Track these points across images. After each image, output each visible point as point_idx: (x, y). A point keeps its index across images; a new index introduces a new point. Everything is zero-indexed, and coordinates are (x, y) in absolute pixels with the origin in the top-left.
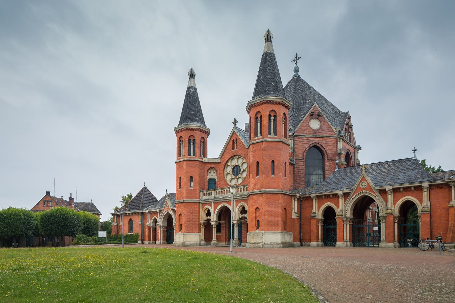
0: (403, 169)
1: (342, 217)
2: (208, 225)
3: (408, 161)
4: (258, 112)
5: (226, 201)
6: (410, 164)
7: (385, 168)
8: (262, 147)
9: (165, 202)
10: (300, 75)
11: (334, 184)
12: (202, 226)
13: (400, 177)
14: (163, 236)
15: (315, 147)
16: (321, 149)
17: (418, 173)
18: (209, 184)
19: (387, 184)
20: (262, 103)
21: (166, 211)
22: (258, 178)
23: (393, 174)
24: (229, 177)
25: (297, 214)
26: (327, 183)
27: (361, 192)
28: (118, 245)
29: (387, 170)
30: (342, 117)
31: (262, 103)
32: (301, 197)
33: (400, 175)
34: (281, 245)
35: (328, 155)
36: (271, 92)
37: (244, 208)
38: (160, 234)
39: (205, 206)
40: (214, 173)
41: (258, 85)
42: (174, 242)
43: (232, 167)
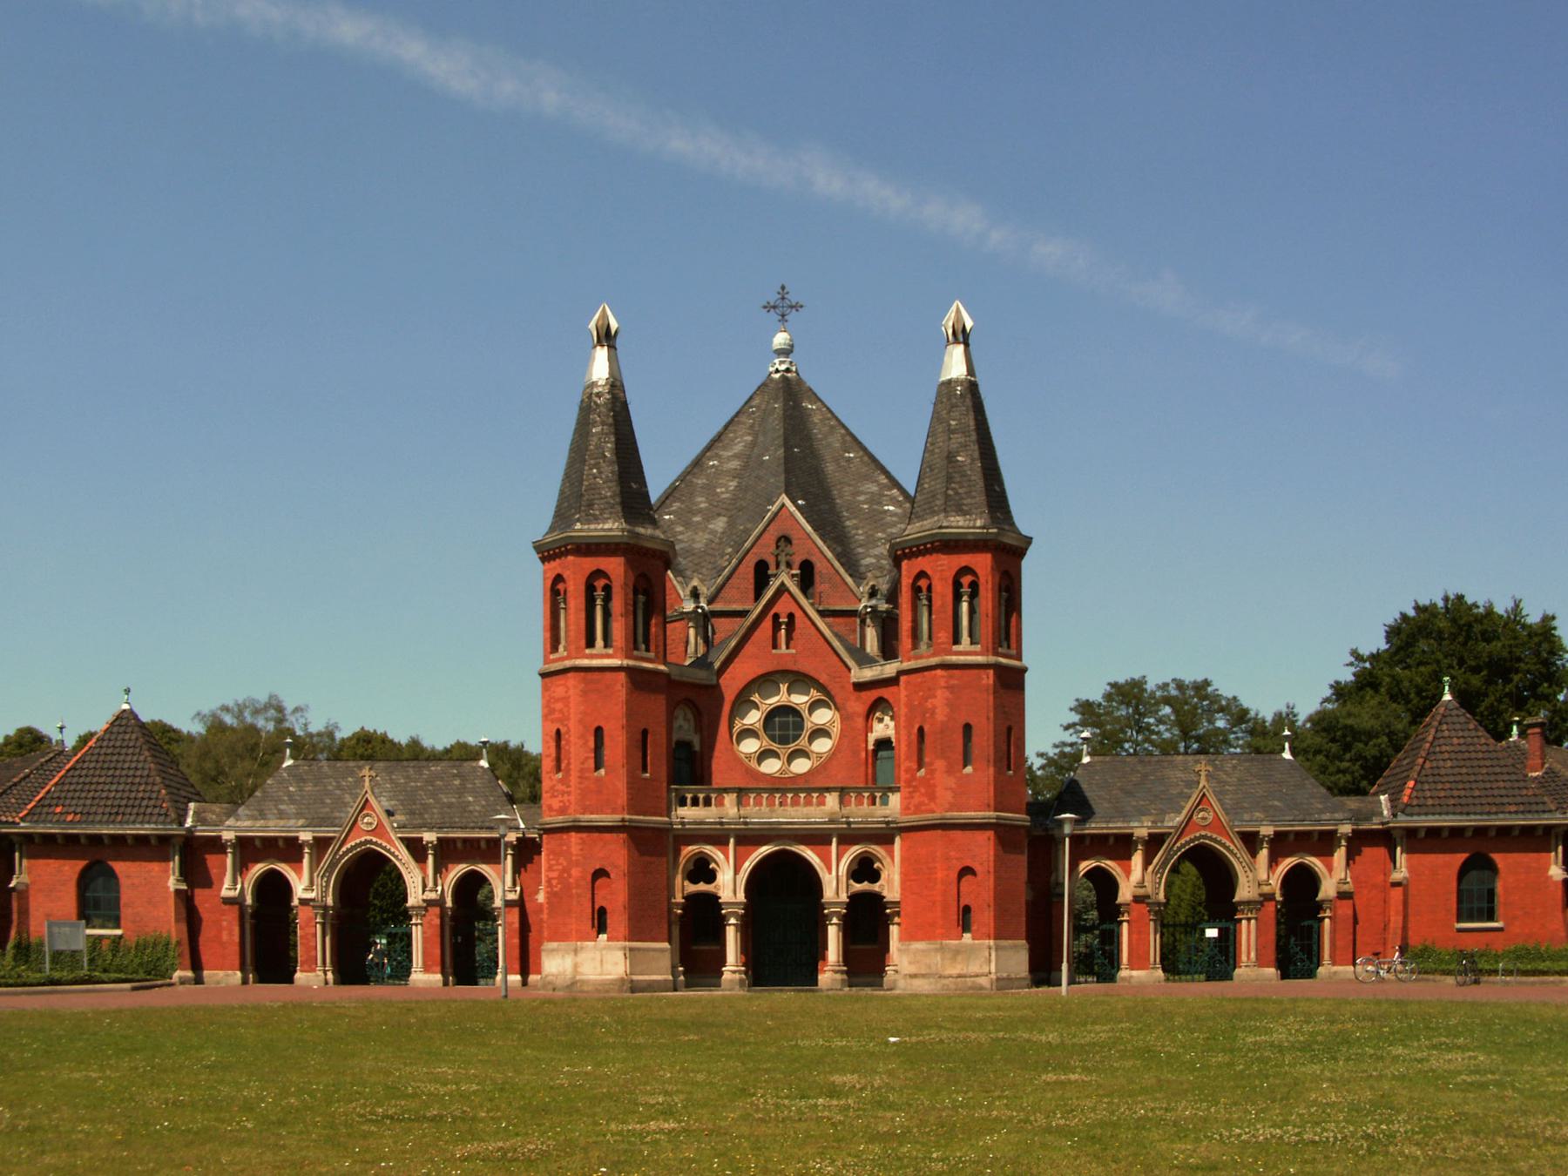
21: (358, 841)
28: (28, 993)
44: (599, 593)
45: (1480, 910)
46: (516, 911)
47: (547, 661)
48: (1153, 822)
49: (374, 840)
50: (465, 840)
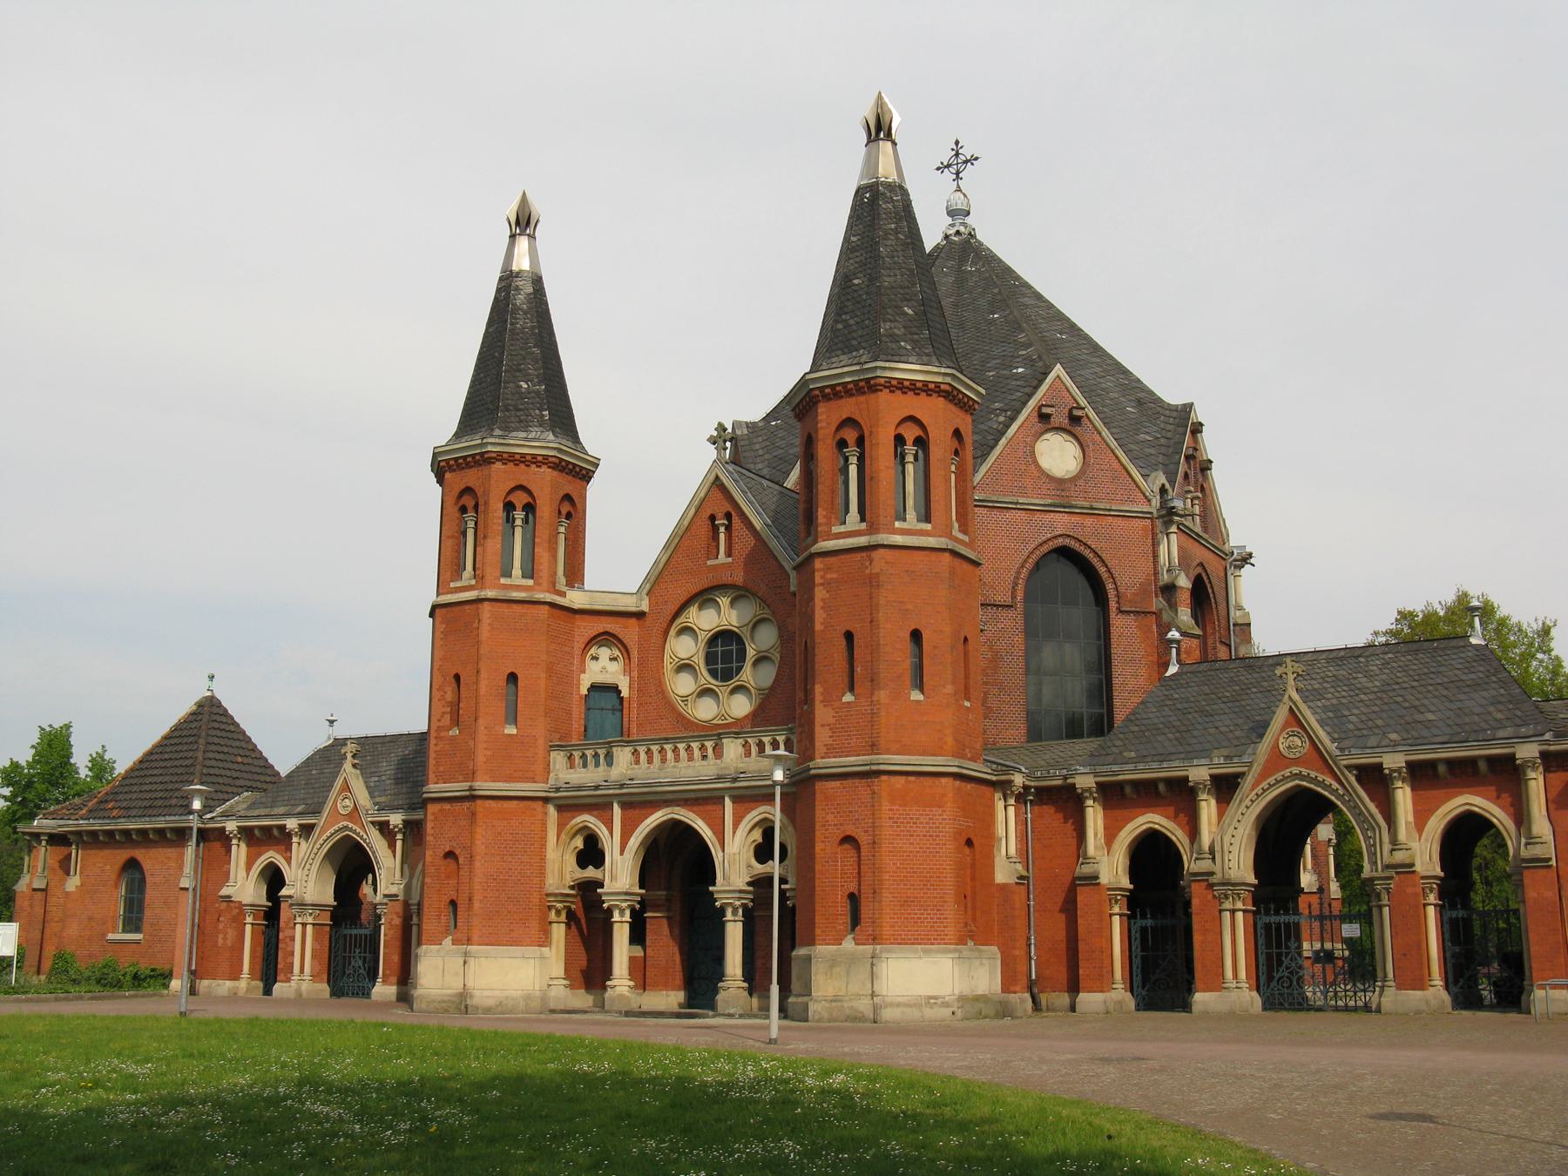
0: (1439, 684)
1: (1213, 880)
3: (1456, 651)
5: (680, 800)
6: (1461, 661)
7: (1369, 675)
8: (868, 571)
10: (974, 229)
11: (1170, 736)
13: (1431, 716)
14: (314, 957)
15: (1065, 553)
16: (1094, 567)
17: (1495, 702)
19: (1383, 743)
22: (849, 703)
23: (1405, 700)
25: (1019, 867)
26: (1136, 729)
27: (1287, 773)
29: (1377, 684)
30: (1171, 427)
32: (1030, 787)
33: (1433, 708)
34: (955, 1009)
35: (1122, 590)
36: (902, 344)
39: (574, 817)
40: (613, 659)
41: (846, 310)
47: (441, 588)
48: (1226, 757)
49: (350, 825)
50: (261, 828)
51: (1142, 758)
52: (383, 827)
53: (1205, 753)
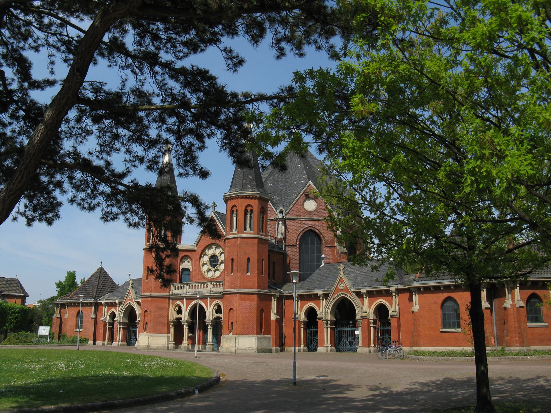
2: (178, 325)
4: (234, 206)
9: (128, 291)
12: (171, 326)
18: (182, 274)
20: (237, 197)
24: (205, 268)
31: (237, 197)
37: (219, 306)
38: (119, 332)
42: (136, 344)
43: (209, 256)
44: (249, 212)
45: (454, 323)
46: (59, 320)
51: (309, 289)
52: (138, 303)
53: (323, 288)
